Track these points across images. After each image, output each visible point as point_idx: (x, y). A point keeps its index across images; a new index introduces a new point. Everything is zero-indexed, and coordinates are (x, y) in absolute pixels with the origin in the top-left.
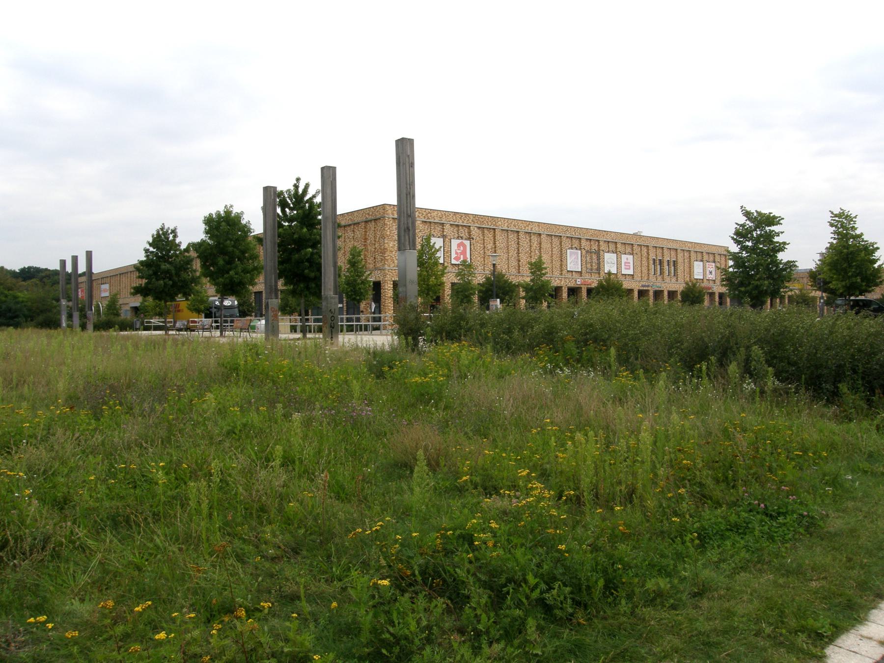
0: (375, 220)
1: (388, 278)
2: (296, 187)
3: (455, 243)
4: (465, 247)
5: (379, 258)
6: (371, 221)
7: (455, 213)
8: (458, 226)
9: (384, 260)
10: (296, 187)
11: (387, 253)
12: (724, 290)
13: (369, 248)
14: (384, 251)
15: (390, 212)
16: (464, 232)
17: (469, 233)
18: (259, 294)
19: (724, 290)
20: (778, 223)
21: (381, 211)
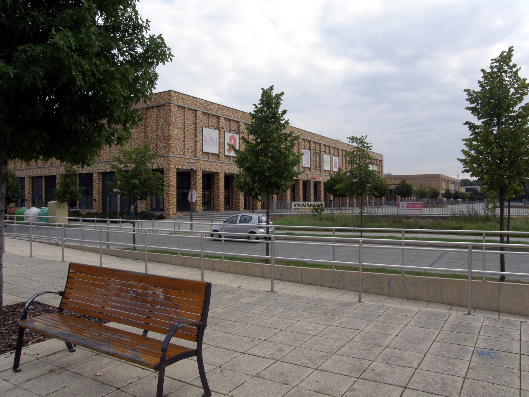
0: (158, 107)
1: (172, 165)
2: (461, 161)
3: (228, 135)
4: (235, 140)
5: (161, 145)
6: (152, 108)
7: (229, 108)
8: (230, 120)
9: (168, 146)
10: (461, 161)
11: (172, 141)
12: (235, 170)
13: (150, 135)
14: (168, 138)
15: (175, 98)
16: (234, 126)
17: (238, 128)
18: (467, 190)
19: (235, 170)
20: (463, 150)
21: (166, 97)
